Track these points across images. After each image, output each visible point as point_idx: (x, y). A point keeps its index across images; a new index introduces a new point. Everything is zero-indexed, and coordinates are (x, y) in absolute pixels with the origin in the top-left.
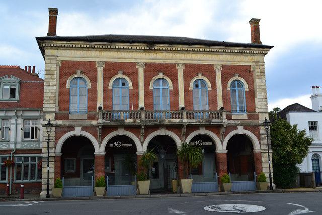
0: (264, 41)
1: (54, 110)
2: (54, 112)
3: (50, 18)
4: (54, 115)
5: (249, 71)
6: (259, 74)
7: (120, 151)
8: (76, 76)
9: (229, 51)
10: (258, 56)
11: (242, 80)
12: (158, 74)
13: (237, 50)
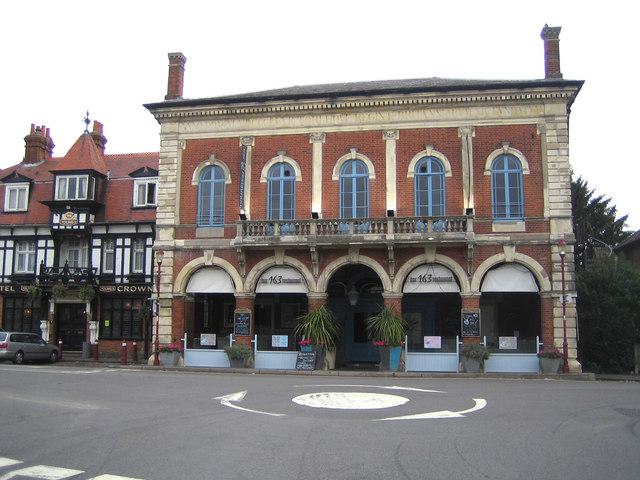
0: (568, 73)
1: (172, 222)
2: (171, 226)
3: (547, 45)
4: (172, 230)
6: (554, 139)
8: (208, 164)
10: (553, 102)
11: (517, 154)
13: (505, 95)
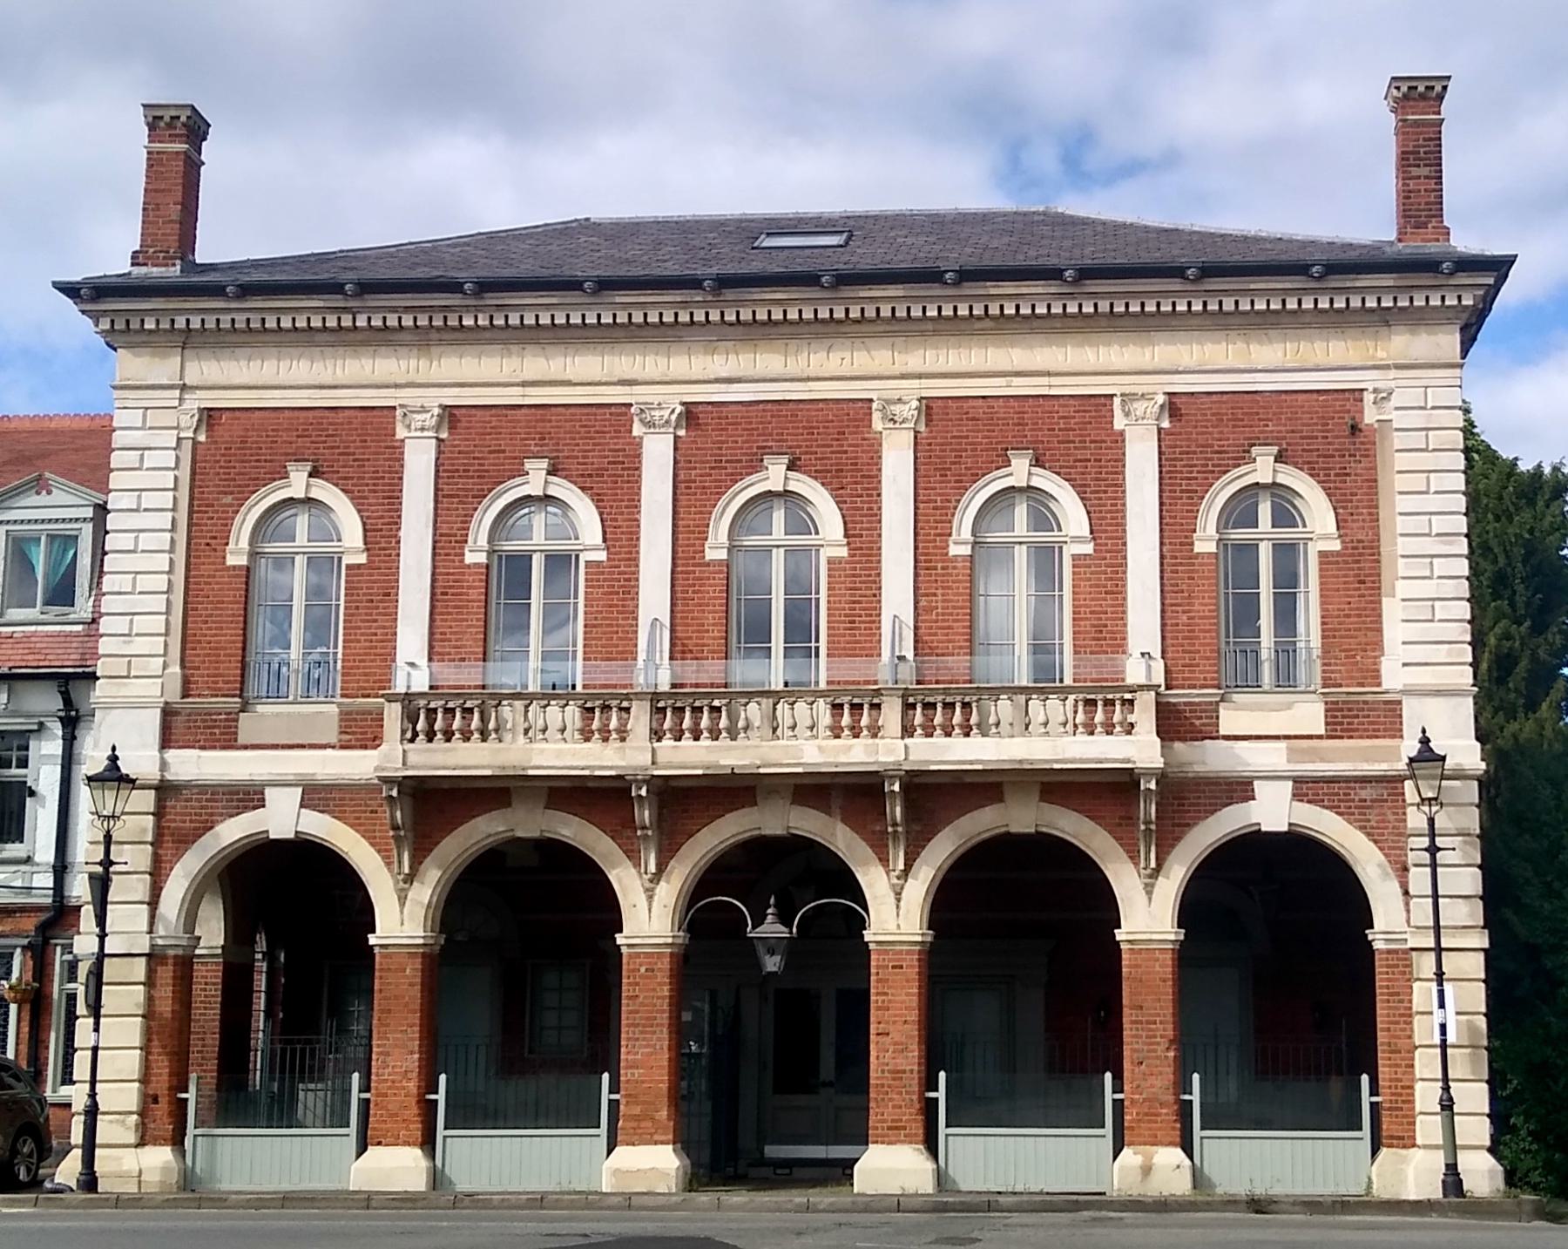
3: (1405, 129)
5: (1355, 429)
7: (526, 925)
9: (271, 323)
12: (755, 466)
